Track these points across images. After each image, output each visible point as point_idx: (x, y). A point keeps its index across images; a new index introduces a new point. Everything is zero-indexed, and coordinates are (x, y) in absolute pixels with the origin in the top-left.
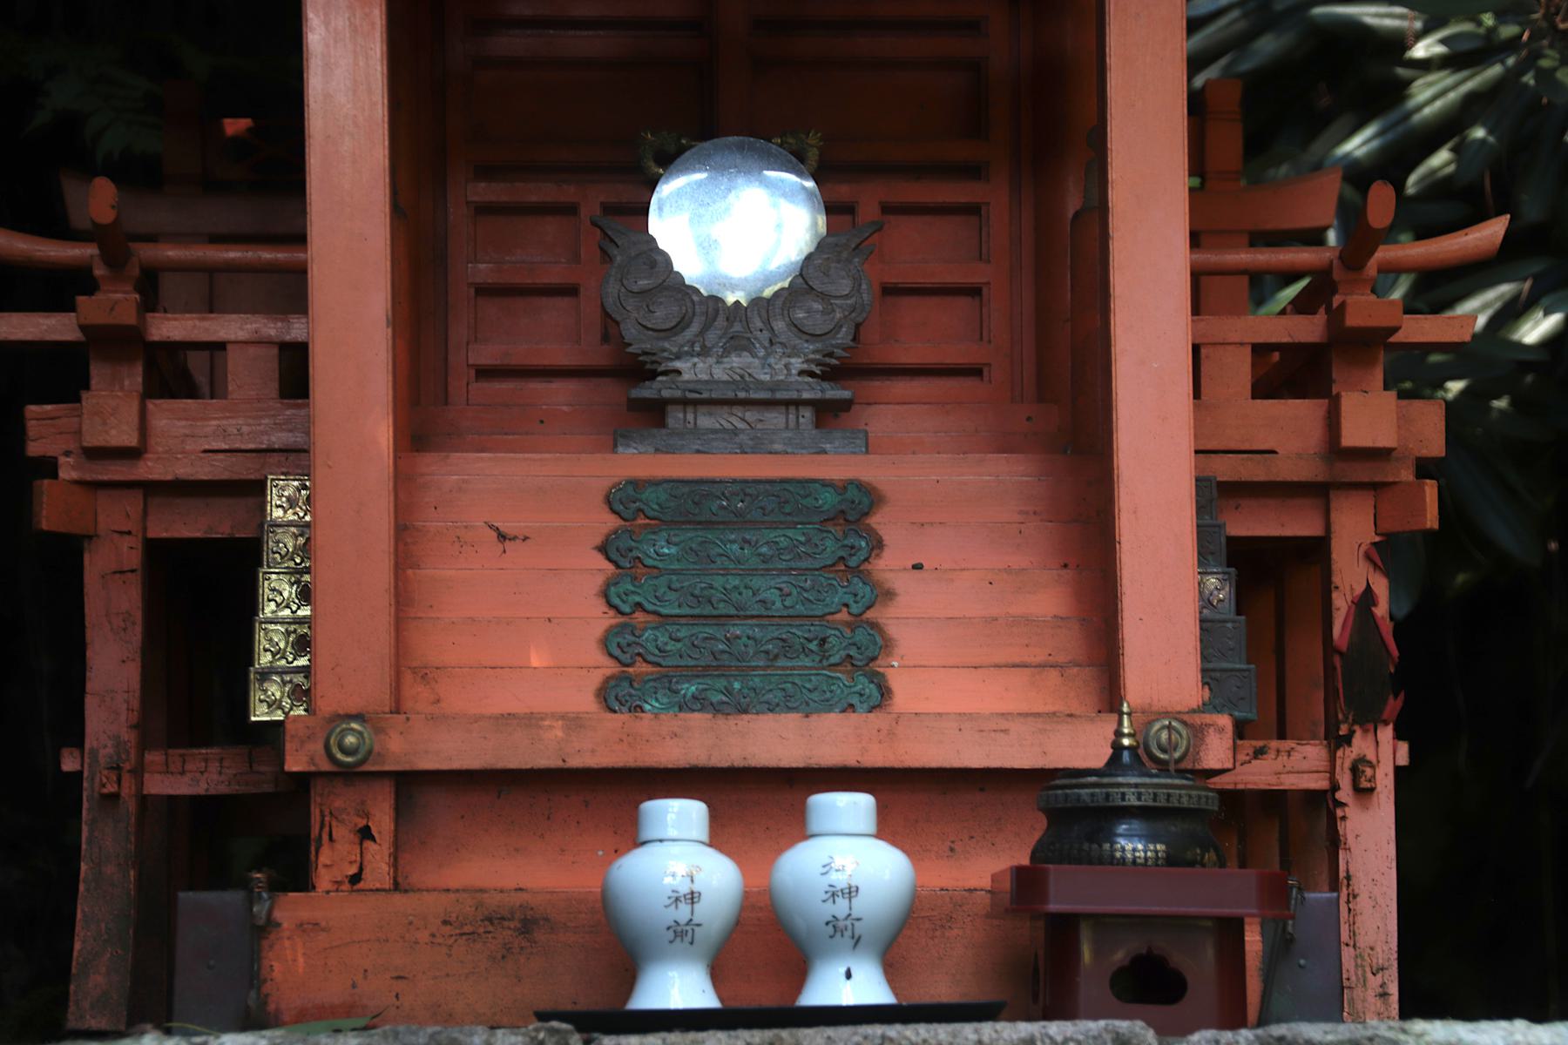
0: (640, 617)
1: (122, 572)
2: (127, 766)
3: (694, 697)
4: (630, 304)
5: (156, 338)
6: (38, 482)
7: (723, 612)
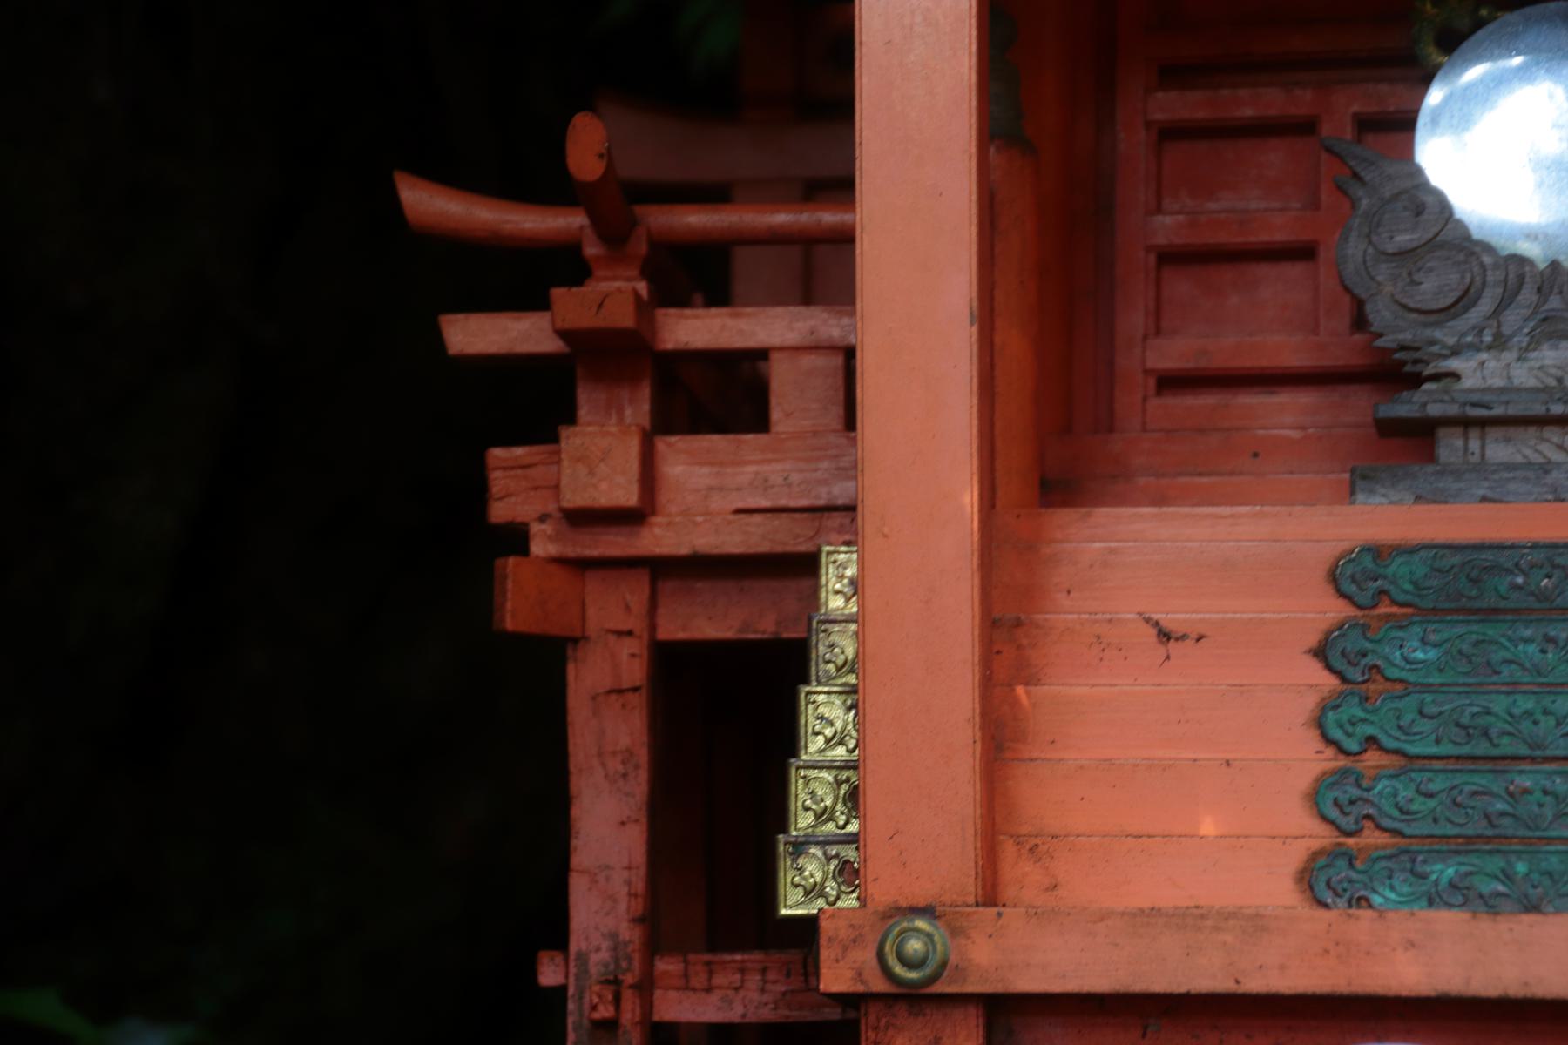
0: (1372, 758)
1: (620, 691)
2: (629, 979)
3: (1452, 885)
4: (1383, 272)
5: (670, 346)
6: (499, 562)
7: (1509, 751)
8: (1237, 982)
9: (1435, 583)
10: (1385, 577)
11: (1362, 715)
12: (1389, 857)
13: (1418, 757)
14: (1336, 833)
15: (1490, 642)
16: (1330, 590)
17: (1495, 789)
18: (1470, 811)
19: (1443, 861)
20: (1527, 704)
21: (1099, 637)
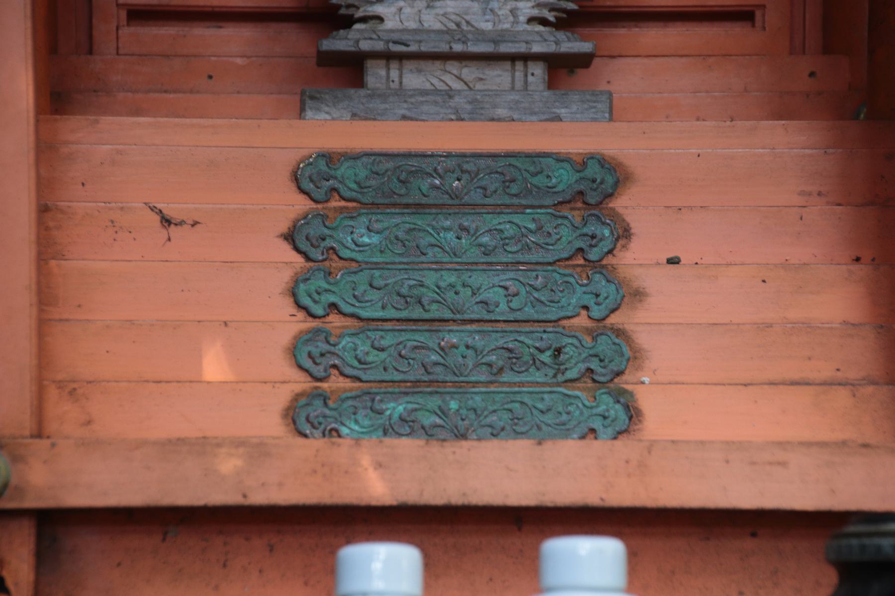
0: (335, 321)
3: (402, 419)
7: (437, 315)
8: (245, 496)
9: (373, 183)
10: (336, 178)
11: (327, 286)
12: (354, 398)
13: (369, 320)
14: (309, 379)
15: (419, 230)
16: (293, 187)
17: (431, 345)
18: (411, 362)
19: (395, 400)
20: (451, 278)
21: (112, 222)
